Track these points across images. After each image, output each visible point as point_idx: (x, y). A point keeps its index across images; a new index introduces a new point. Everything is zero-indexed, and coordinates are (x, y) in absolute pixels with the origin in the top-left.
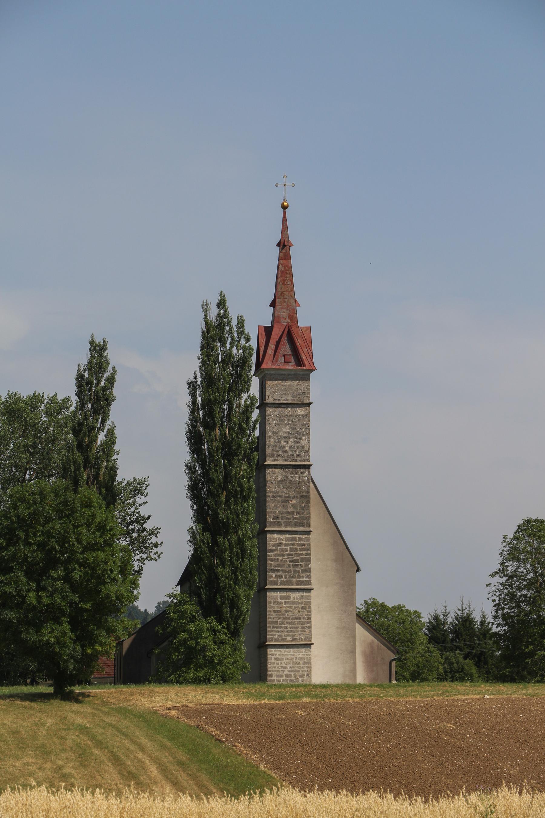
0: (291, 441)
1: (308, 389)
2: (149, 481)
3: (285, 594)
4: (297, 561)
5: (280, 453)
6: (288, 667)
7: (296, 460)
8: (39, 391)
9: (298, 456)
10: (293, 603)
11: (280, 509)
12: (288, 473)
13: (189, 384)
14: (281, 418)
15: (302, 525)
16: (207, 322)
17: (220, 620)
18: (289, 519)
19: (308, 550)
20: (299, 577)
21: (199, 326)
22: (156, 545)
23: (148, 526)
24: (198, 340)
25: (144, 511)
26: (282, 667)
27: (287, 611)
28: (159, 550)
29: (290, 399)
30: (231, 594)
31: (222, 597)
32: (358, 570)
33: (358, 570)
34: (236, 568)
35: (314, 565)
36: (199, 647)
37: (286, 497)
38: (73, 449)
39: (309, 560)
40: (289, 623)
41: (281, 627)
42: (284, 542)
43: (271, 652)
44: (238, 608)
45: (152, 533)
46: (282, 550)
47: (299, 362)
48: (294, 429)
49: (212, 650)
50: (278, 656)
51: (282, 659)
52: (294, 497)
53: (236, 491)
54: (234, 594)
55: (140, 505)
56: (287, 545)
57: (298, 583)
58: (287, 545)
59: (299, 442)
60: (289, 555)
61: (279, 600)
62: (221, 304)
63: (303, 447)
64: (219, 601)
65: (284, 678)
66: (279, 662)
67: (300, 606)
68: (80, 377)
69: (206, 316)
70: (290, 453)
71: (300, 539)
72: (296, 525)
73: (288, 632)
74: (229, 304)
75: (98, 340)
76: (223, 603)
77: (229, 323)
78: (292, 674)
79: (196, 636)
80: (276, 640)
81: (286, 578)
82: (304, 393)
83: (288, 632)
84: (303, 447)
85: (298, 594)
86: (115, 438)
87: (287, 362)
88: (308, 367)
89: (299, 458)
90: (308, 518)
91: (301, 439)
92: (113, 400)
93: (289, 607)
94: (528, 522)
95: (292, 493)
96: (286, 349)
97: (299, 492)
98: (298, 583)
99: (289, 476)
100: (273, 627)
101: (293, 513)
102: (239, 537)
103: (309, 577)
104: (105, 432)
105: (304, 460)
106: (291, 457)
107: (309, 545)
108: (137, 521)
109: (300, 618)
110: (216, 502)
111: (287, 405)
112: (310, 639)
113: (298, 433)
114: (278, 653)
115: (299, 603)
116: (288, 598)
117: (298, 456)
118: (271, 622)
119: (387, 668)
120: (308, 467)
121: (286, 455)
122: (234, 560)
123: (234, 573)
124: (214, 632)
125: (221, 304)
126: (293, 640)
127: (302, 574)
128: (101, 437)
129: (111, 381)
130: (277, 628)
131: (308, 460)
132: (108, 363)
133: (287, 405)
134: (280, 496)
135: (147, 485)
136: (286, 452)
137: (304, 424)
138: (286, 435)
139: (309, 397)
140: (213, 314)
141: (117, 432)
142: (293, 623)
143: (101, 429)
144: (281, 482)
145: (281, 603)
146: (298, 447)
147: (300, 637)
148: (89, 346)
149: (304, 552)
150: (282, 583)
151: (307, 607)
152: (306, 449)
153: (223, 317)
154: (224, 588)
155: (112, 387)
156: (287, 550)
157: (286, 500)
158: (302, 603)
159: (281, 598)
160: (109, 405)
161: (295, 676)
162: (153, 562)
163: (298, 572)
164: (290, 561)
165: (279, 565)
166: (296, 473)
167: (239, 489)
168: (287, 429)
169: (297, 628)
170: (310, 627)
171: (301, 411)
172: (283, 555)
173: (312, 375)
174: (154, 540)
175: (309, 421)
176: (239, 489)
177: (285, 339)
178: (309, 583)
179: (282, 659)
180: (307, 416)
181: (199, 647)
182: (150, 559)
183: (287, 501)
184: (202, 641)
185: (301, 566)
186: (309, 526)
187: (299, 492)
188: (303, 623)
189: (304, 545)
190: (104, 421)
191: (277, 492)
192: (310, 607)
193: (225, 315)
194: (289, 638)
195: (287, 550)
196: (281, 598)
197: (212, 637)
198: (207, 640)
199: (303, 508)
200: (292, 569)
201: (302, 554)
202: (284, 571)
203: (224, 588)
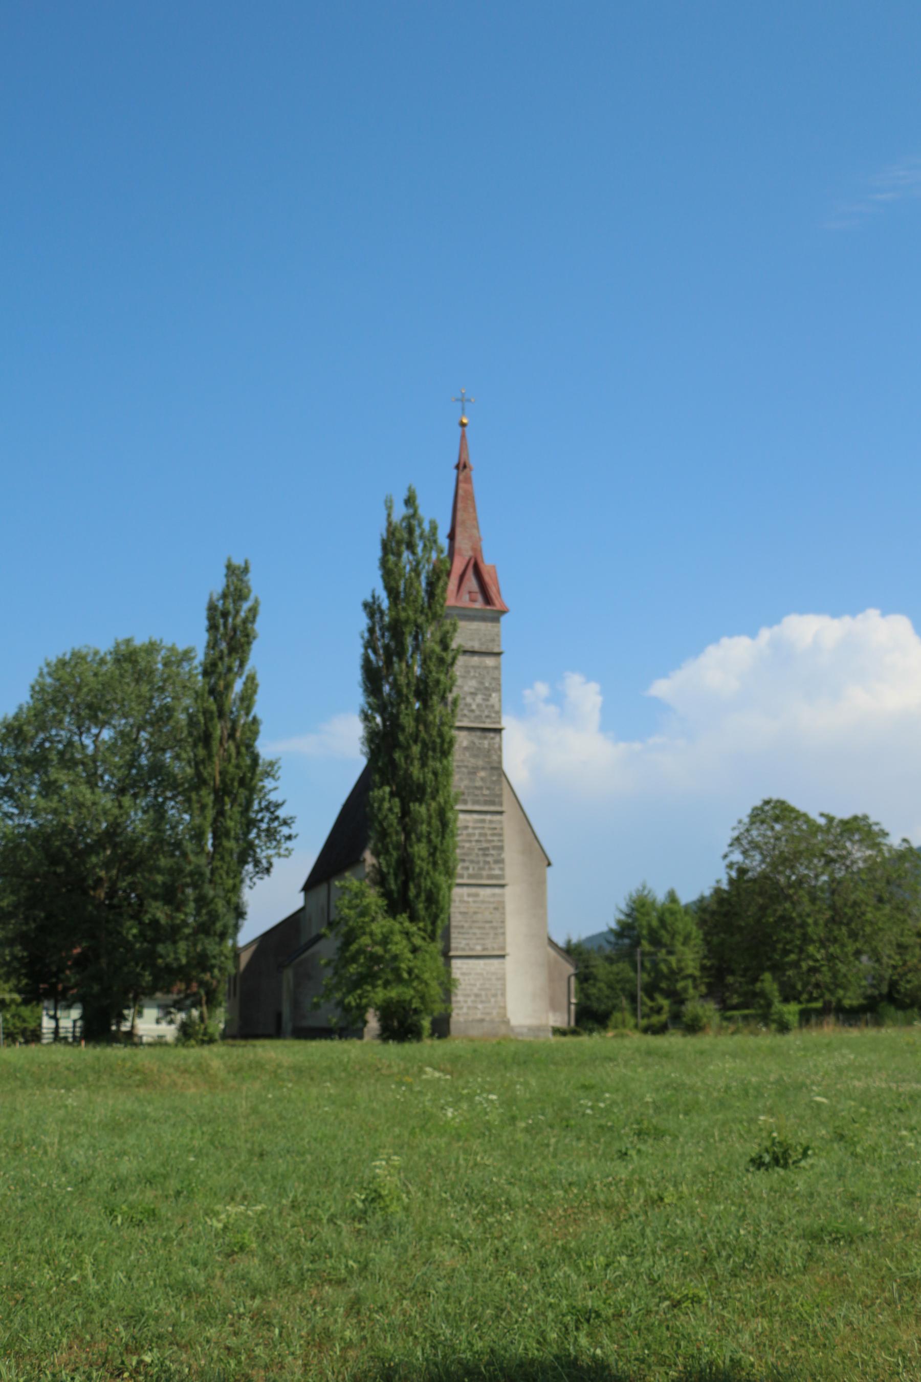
0: (479, 698)
1: (498, 635)
2: (281, 763)
3: (474, 890)
4: (487, 849)
5: (466, 712)
6: (478, 984)
7: (484, 722)
8: (156, 638)
9: (488, 717)
10: (483, 902)
11: (466, 783)
12: (475, 737)
13: (366, 605)
14: (467, 668)
15: (492, 803)
16: (390, 524)
17: (413, 918)
18: (477, 795)
19: (500, 835)
20: (491, 869)
21: (379, 530)
22: (289, 838)
23: (282, 813)
24: (377, 552)
25: (273, 797)
26: (470, 985)
27: (475, 913)
28: (289, 844)
29: (476, 646)
30: (429, 883)
31: (418, 886)
32: (549, 864)
33: (549, 864)
34: (435, 848)
35: (507, 855)
36: (387, 956)
37: (473, 768)
38: (203, 695)
39: (501, 848)
40: (479, 928)
41: (468, 933)
42: (471, 824)
43: (456, 964)
44: (437, 902)
45: (285, 823)
46: (469, 835)
47: (488, 600)
48: (482, 683)
49: (407, 961)
50: (464, 971)
51: (470, 974)
52: (483, 769)
53: (434, 742)
54: (432, 883)
55: (270, 791)
56: (475, 828)
57: (490, 877)
58: (475, 828)
59: (488, 700)
60: (477, 841)
61: (466, 898)
62: (410, 501)
63: (493, 706)
64: (412, 892)
65: (473, 998)
66: (466, 978)
67: (492, 906)
68: (212, 608)
69: (389, 515)
70: (477, 713)
71: (491, 822)
72: (486, 803)
73: (478, 939)
74: (420, 501)
75: (238, 562)
76: (418, 896)
77: (420, 524)
78: (483, 993)
79: (385, 941)
80: (463, 949)
81: (474, 869)
82: (493, 640)
83: (478, 939)
84: (493, 706)
85: (489, 891)
86: (257, 686)
87: (473, 600)
88: (498, 607)
89: (488, 720)
90: (500, 796)
91: (490, 695)
92: (254, 638)
93: (479, 908)
94: (782, 803)
95: (480, 763)
96: (471, 583)
97: (489, 763)
98: (490, 877)
99: (477, 741)
100: (459, 933)
101: (481, 788)
102: (439, 804)
103: (502, 869)
104: (244, 678)
105: (494, 723)
106: (478, 718)
107: (502, 829)
108: (267, 808)
109: (491, 922)
110: (407, 757)
111: (473, 653)
112: (503, 948)
113: (487, 689)
114: (465, 966)
115: (489, 902)
116: (477, 895)
117: (488, 717)
118: (456, 927)
119: (565, 984)
120: (498, 731)
121: (472, 715)
122: (433, 836)
123: (432, 854)
124: (407, 934)
125: (410, 501)
126: (484, 949)
127: (493, 866)
128: (238, 686)
129: (253, 611)
130: (463, 933)
131: (499, 722)
132: (249, 591)
133: (473, 653)
134: (466, 767)
135: (279, 768)
136: (472, 711)
137: (494, 679)
138: (472, 690)
139: (499, 646)
140: (400, 512)
141: (260, 679)
142: (484, 928)
143: (239, 674)
144: (466, 748)
145: (468, 902)
146: (487, 706)
147: (492, 947)
148: (224, 571)
149: (495, 838)
150: (470, 876)
151: (499, 907)
152: (497, 708)
153: (413, 517)
154: (420, 874)
155: (253, 621)
156: (474, 834)
157: (473, 772)
158: (493, 903)
159: (469, 895)
160: (249, 643)
161: (486, 995)
162: (282, 859)
163: (488, 863)
164: (480, 849)
165: (465, 854)
166: (485, 738)
167: (438, 740)
168: (473, 683)
169: (487, 934)
170: (504, 934)
171: (490, 661)
172: (470, 841)
173: (504, 619)
174: (285, 831)
175: (500, 674)
176: (438, 740)
177: (470, 573)
178: (501, 877)
179: (470, 974)
180: (497, 668)
181: (387, 956)
182: (279, 855)
183: (475, 773)
184: (394, 949)
185: (492, 855)
186: (501, 804)
187: (489, 763)
188: (495, 928)
189: (495, 829)
190: (242, 665)
191: (462, 761)
192: (504, 908)
193: (414, 515)
194: (479, 948)
195: (474, 834)
196: (469, 895)
197: (405, 942)
198: (399, 946)
199: (493, 782)
200: (481, 859)
201: (493, 841)
202: (472, 862)
203: (420, 874)
